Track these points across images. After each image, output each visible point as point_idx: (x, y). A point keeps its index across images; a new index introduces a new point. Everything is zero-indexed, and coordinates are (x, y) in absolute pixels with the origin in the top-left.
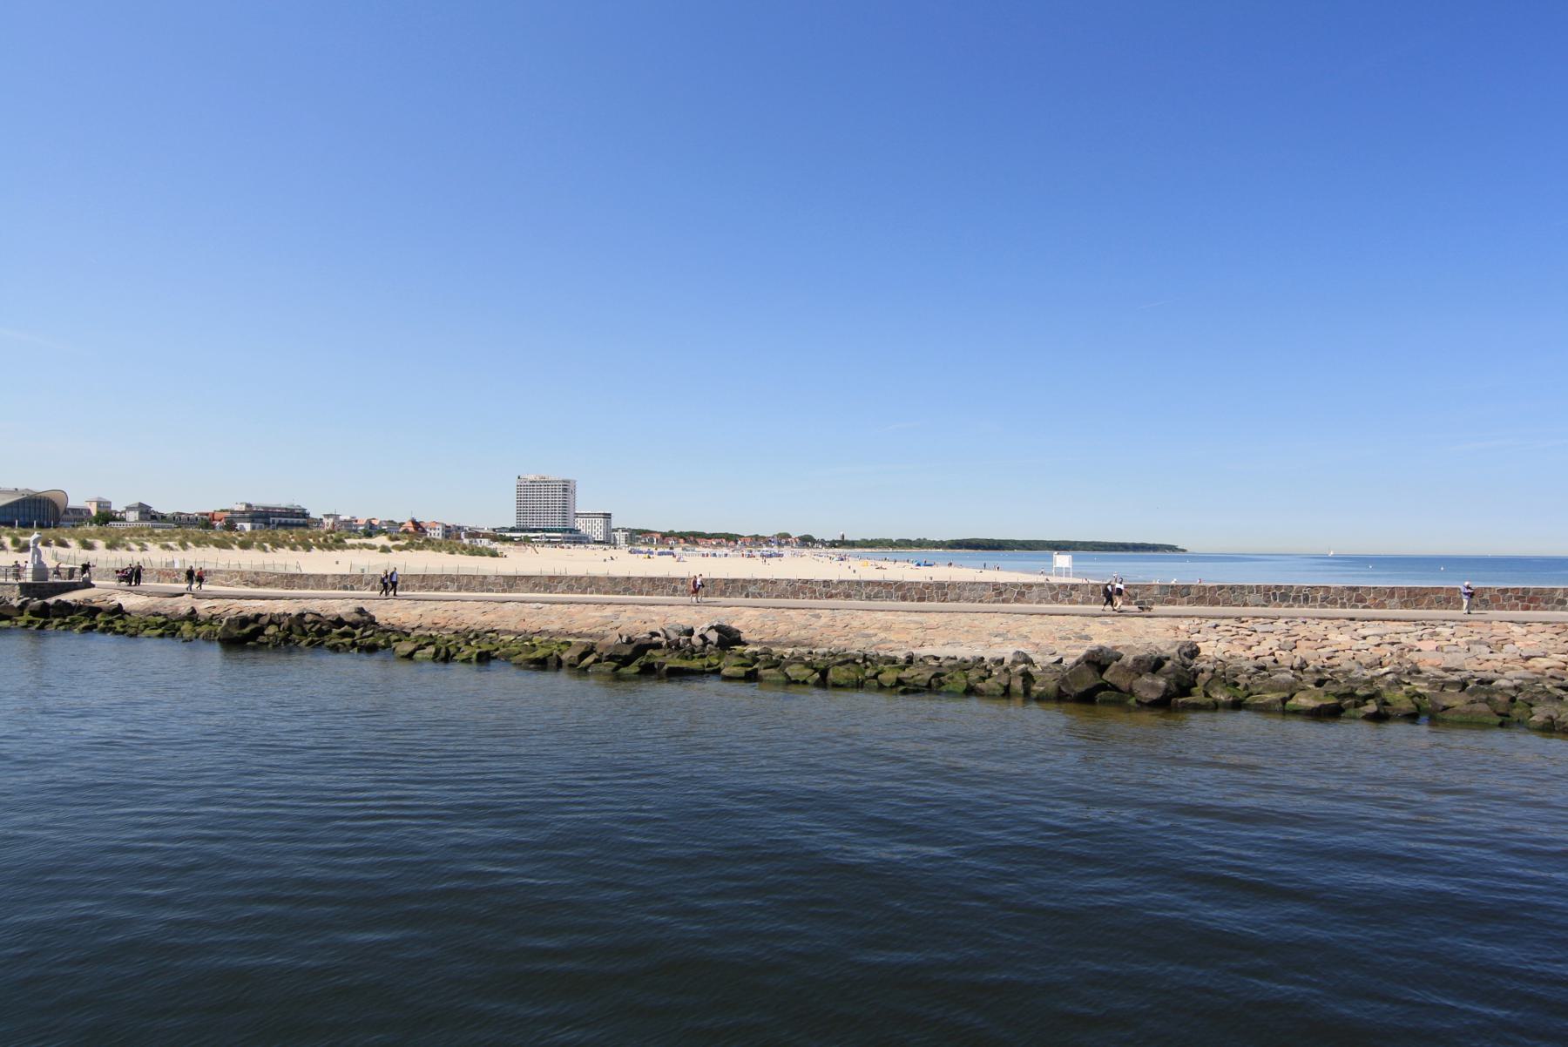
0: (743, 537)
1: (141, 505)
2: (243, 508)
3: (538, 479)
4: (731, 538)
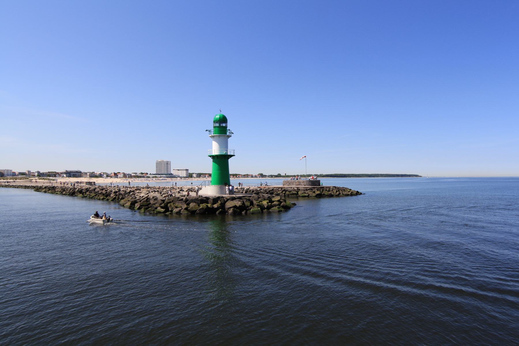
0: (312, 175)
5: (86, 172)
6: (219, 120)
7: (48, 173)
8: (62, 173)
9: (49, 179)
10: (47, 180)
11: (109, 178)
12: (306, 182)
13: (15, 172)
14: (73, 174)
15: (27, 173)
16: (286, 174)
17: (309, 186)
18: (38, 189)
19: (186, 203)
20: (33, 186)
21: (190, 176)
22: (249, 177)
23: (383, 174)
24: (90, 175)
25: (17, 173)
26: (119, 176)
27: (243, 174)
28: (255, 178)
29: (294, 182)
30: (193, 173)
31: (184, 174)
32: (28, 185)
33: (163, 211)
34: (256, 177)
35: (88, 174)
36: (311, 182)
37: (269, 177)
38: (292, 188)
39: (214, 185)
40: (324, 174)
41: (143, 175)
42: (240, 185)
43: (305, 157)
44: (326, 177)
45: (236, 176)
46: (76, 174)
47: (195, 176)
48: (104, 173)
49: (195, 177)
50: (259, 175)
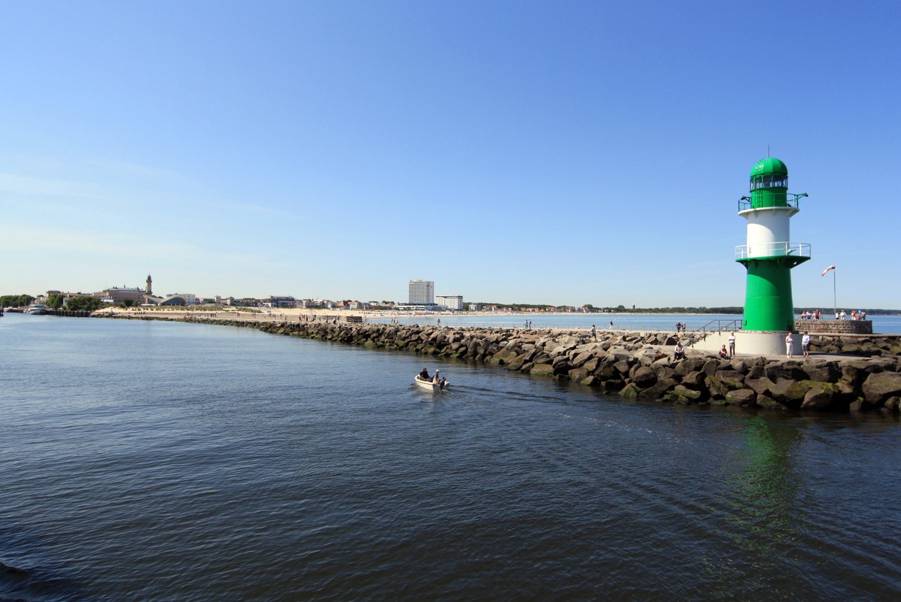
1: (231, 297)
2: (270, 298)
3: (418, 281)
4: (527, 307)
5: (302, 299)
6: (772, 171)
7: (246, 301)
8: (265, 301)
9: (252, 311)
10: (249, 312)
11: (339, 309)
12: (843, 325)
13: (199, 297)
14: (282, 303)
15: (216, 300)
16: (634, 306)
17: (851, 333)
18: (269, 328)
19: (439, 351)
20: (250, 323)
21: (465, 307)
22: (568, 312)
23: (719, 309)
24: (307, 304)
25: (201, 300)
26: (351, 306)
27: (556, 306)
28: (580, 314)
29: (812, 324)
30: (470, 303)
31: (455, 304)
32: (241, 321)
33: (695, 395)
34: (580, 310)
35: (304, 302)
36: (856, 325)
37: (604, 311)
38: (820, 337)
39: (760, 330)
40: (708, 307)
41: (386, 306)
42: (679, 328)
43: (833, 268)
44: (713, 313)
45: (545, 309)
46: (286, 302)
47: (474, 309)
48: (328, 301)
49: (473, 310)
50: (585, 306)
